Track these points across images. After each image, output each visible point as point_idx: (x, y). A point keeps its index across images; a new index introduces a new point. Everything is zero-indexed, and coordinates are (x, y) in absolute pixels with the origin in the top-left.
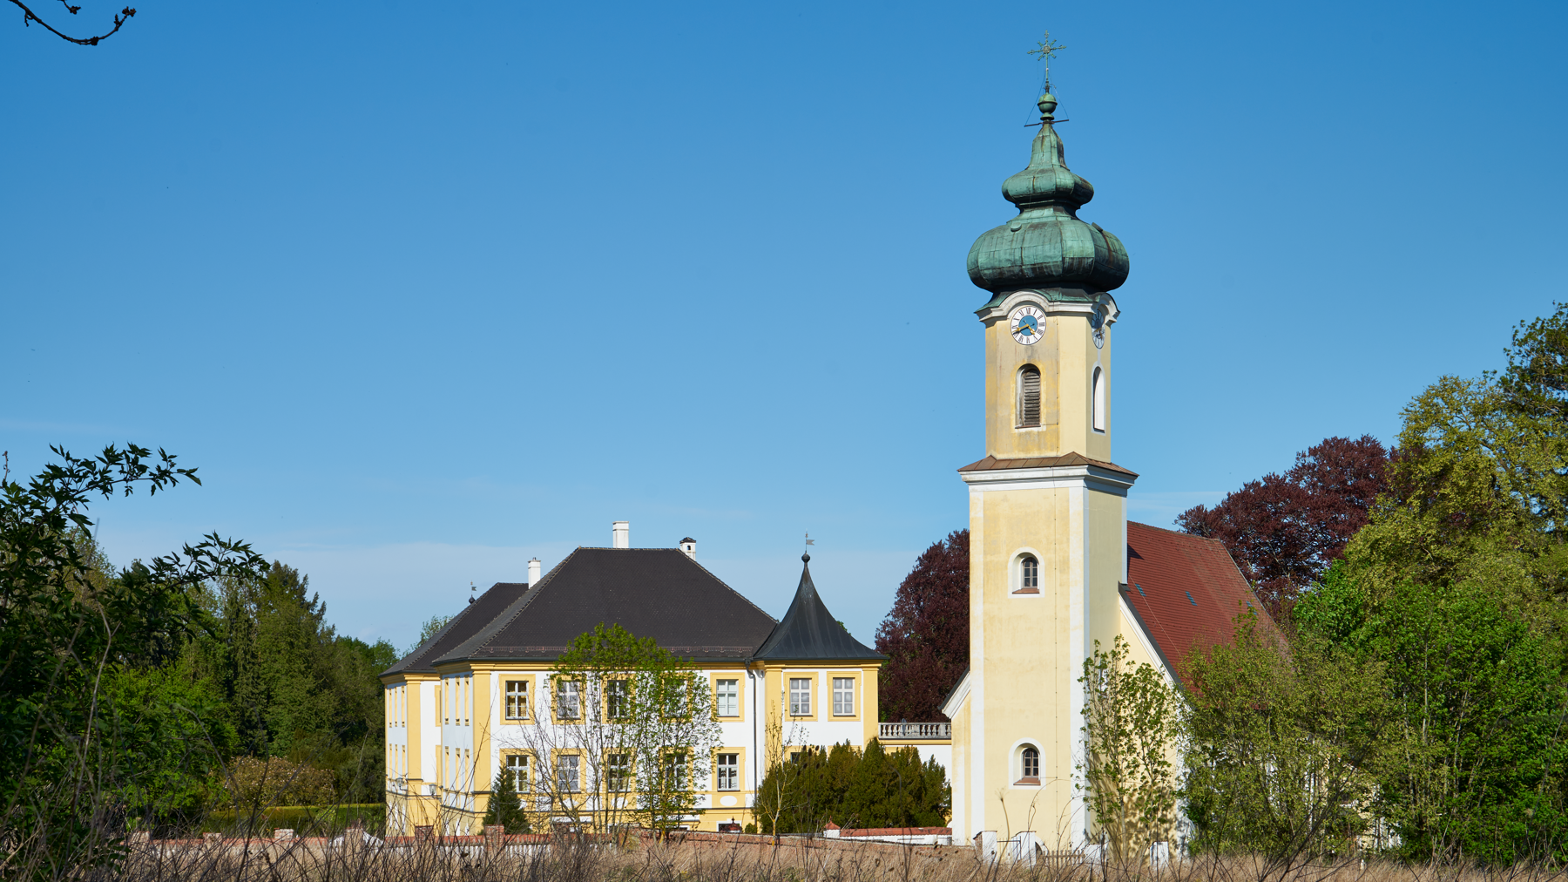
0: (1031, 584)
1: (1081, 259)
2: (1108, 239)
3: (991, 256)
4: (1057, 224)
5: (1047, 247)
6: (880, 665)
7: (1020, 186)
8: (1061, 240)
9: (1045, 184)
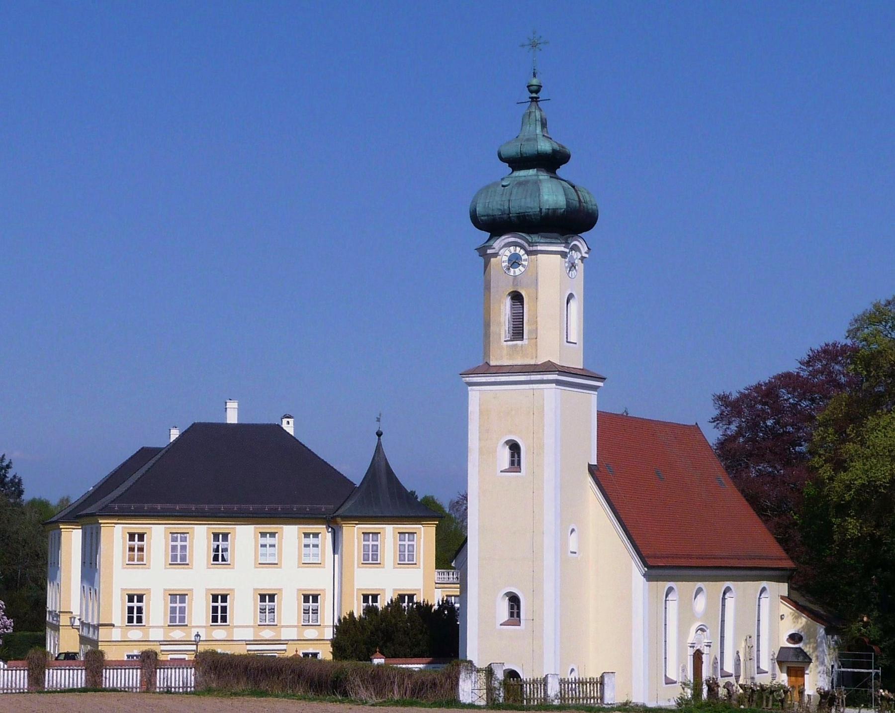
0: (516, 465)
1: (555, 210)
2: (579, 192)
3: (487, 206)
4: (537, 183)
5: (528, 200)
6: (438, 522)
7: (512, 150)
8: (539, 195)
9: (529, 149)
